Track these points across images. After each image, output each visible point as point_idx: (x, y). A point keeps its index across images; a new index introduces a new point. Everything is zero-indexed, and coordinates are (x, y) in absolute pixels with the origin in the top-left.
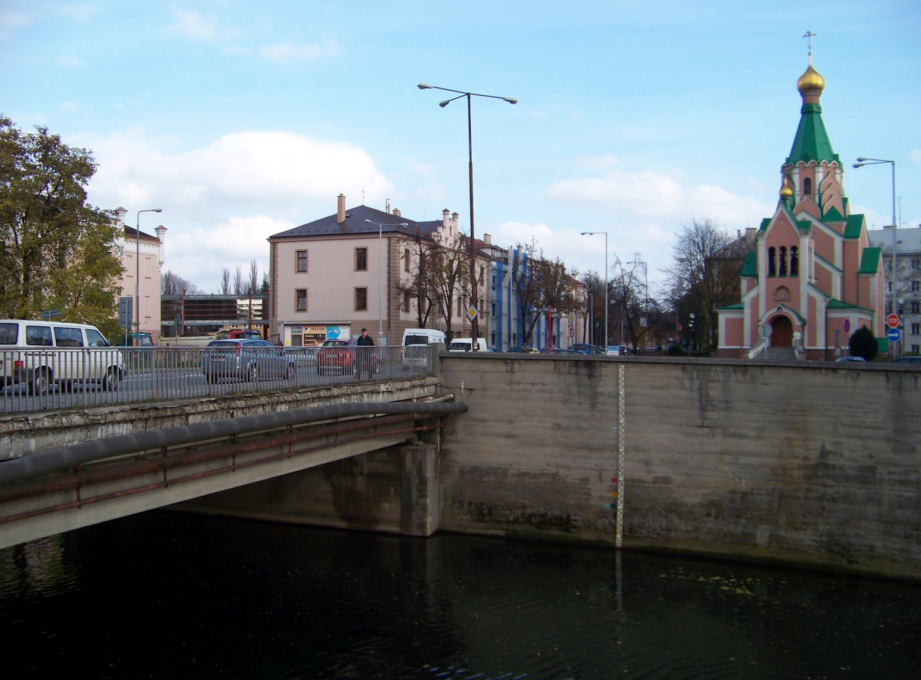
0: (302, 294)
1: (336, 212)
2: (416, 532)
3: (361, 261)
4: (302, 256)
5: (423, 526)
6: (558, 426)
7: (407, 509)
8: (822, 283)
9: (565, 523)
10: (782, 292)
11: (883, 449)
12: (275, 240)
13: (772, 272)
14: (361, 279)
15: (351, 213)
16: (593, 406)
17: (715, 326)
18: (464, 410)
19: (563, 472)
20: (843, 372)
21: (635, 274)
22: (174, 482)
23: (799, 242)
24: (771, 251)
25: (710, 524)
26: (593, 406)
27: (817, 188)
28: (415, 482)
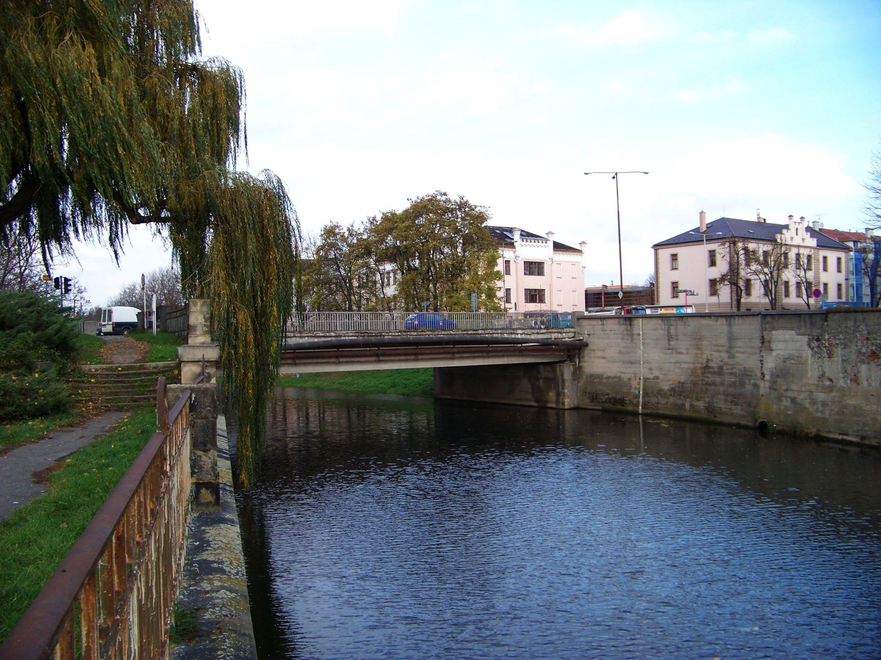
0: (675, 285)
1: (698, 225)
2: (561, 407)
4: (674, 257)
5: (563, 403)
6: (620, 352)
7: (558, 394)
9: (622, 401)
11: (724, 355)
12: (657, 247)
15: (710, 226)
16: (632, 340)
18: (586, 345)
19: (623, 376)
22: (383, 361)
25: (672, 400)
26: (632, 340)
28: (560, 380)
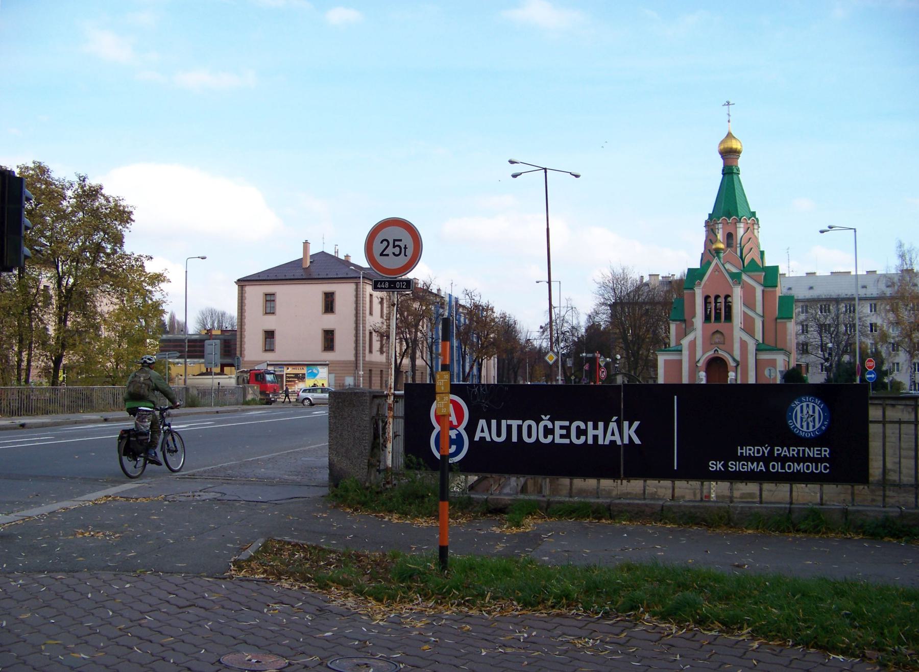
0: (269, 335)
1: (301, 256)
3: (329, 304)
4: (270, 299)
8: (748, 328)
10: (718, 335)
12: (243, 283)
13: (707, 318)
14: (329, 322)
17: (655, 366)
20: (900, 407)
21: (567, 317)
23: (732, 292)
24: (707, 298)
27: (739, 242)
